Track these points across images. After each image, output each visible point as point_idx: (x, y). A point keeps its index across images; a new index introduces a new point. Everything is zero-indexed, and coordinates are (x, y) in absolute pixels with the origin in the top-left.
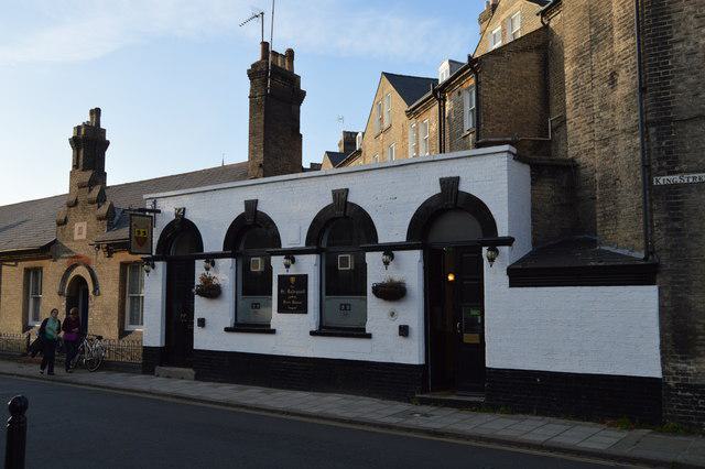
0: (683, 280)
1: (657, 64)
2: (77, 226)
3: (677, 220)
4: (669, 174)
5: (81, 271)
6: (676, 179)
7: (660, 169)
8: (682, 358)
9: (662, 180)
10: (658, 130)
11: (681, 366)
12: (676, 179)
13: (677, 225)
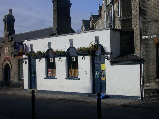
0: (148, 63)
1: (143, 7)
2: (6, 48)
3: (147, 48)
4: (146, 35)
5: (7, 62)
6: (147, 37)
7: (144, 34)
8: (148, 83)
9: (144, 37)
10: (143, 24)
11: (148, 85)
12: (147, 37)
13: (147, 49)
